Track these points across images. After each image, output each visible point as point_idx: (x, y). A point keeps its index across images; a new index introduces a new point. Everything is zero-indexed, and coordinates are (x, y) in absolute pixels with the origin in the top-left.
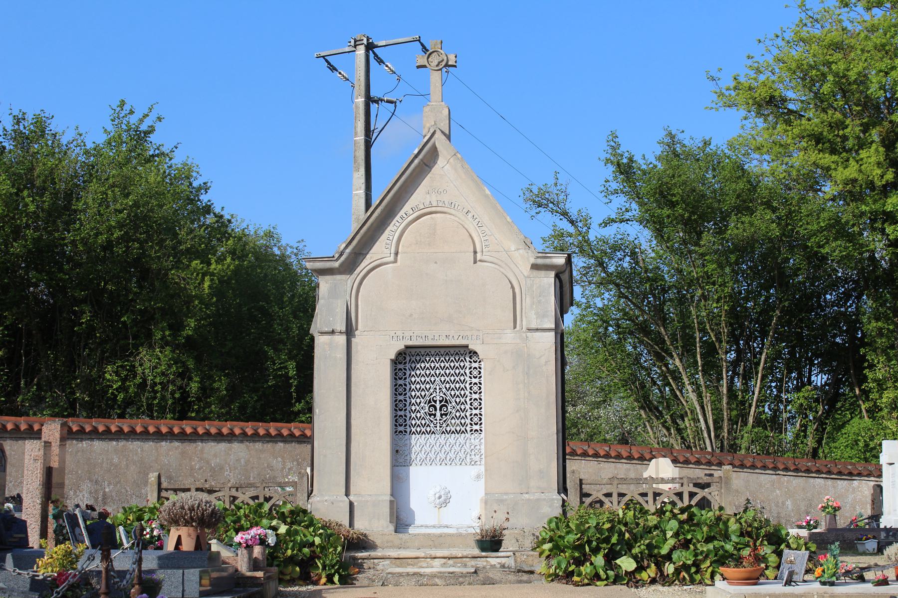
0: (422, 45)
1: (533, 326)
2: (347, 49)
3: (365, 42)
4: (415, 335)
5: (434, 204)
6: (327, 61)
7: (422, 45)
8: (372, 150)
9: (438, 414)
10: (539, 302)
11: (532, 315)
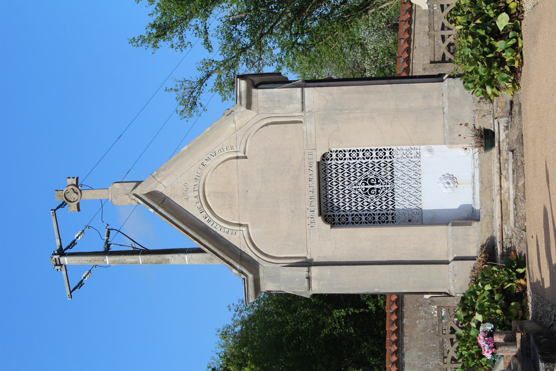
0: (58, 208)
1: (299, 106)
7: (58, 208)
8: (150, 248)
9: (377, 186)
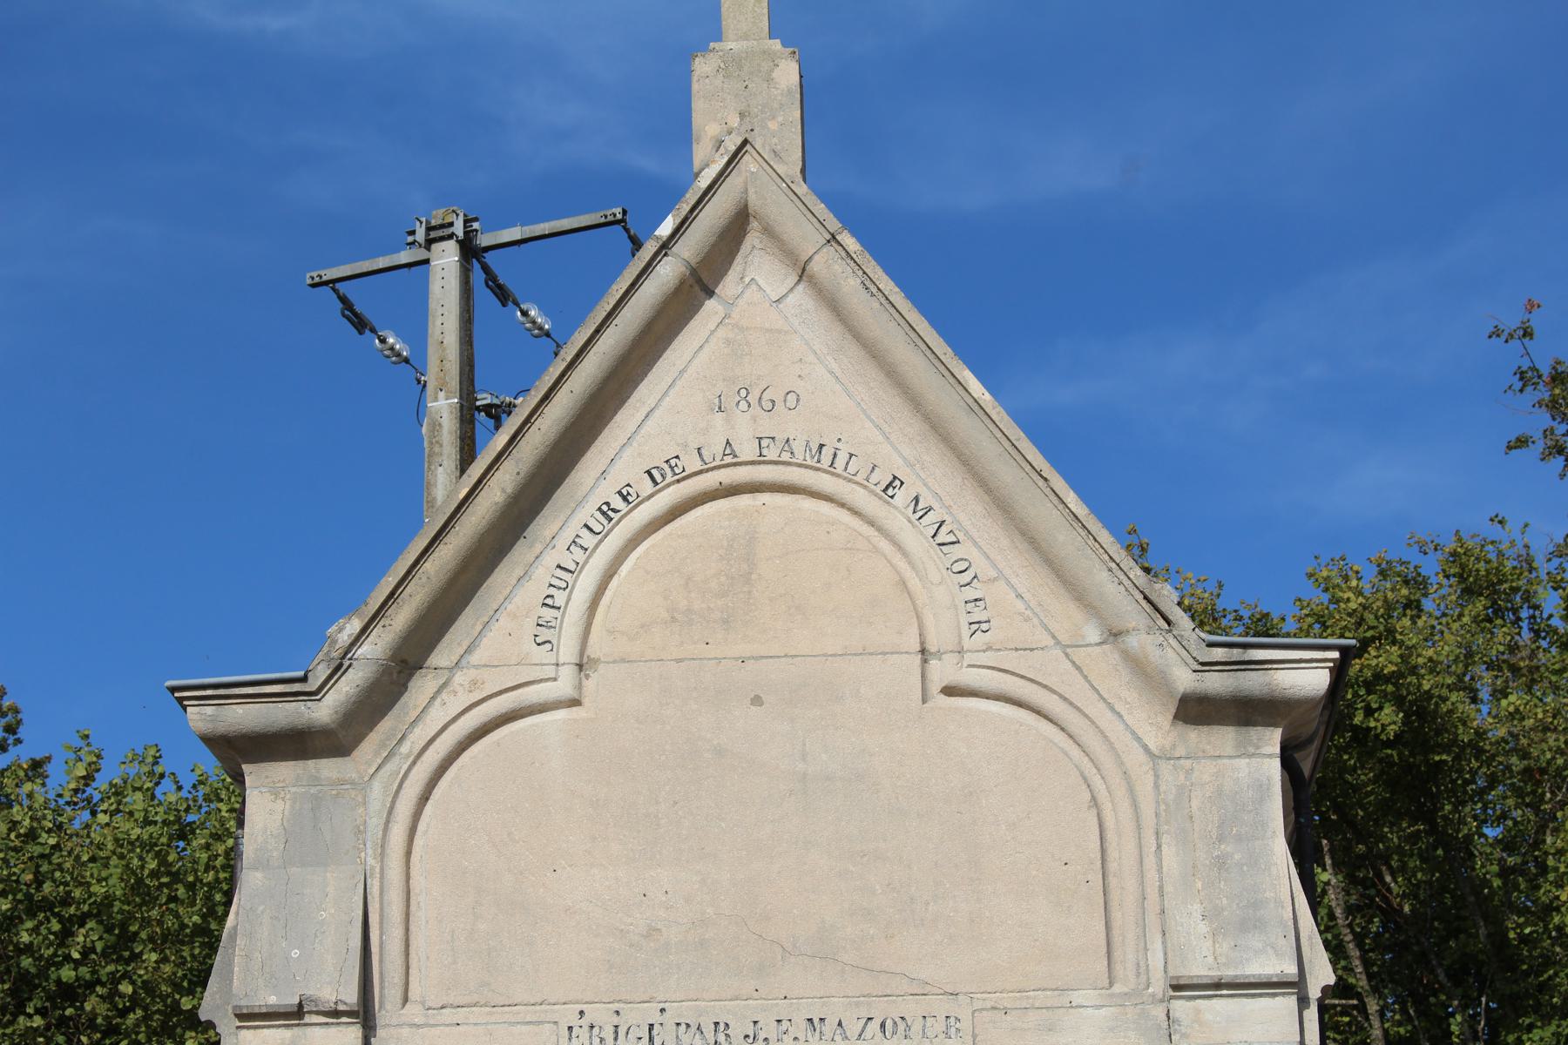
1: (1200, 969)
2: (405, 257)
3: (458, 229)
4: (669, 1019)
5: (747, 451)
6: (344, 300)
10: (1221, 863)
11: (1191, 924)
